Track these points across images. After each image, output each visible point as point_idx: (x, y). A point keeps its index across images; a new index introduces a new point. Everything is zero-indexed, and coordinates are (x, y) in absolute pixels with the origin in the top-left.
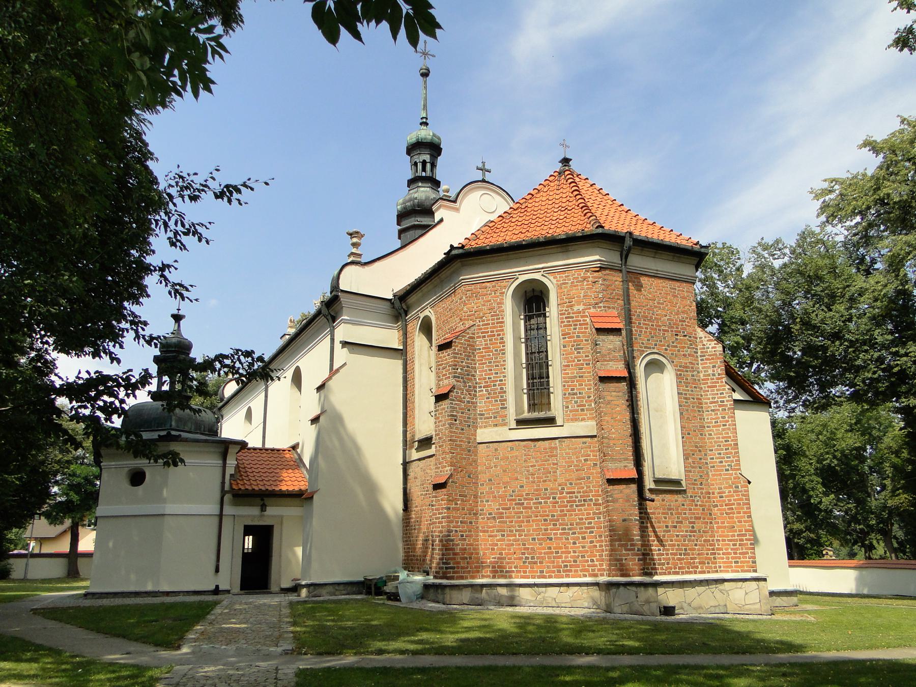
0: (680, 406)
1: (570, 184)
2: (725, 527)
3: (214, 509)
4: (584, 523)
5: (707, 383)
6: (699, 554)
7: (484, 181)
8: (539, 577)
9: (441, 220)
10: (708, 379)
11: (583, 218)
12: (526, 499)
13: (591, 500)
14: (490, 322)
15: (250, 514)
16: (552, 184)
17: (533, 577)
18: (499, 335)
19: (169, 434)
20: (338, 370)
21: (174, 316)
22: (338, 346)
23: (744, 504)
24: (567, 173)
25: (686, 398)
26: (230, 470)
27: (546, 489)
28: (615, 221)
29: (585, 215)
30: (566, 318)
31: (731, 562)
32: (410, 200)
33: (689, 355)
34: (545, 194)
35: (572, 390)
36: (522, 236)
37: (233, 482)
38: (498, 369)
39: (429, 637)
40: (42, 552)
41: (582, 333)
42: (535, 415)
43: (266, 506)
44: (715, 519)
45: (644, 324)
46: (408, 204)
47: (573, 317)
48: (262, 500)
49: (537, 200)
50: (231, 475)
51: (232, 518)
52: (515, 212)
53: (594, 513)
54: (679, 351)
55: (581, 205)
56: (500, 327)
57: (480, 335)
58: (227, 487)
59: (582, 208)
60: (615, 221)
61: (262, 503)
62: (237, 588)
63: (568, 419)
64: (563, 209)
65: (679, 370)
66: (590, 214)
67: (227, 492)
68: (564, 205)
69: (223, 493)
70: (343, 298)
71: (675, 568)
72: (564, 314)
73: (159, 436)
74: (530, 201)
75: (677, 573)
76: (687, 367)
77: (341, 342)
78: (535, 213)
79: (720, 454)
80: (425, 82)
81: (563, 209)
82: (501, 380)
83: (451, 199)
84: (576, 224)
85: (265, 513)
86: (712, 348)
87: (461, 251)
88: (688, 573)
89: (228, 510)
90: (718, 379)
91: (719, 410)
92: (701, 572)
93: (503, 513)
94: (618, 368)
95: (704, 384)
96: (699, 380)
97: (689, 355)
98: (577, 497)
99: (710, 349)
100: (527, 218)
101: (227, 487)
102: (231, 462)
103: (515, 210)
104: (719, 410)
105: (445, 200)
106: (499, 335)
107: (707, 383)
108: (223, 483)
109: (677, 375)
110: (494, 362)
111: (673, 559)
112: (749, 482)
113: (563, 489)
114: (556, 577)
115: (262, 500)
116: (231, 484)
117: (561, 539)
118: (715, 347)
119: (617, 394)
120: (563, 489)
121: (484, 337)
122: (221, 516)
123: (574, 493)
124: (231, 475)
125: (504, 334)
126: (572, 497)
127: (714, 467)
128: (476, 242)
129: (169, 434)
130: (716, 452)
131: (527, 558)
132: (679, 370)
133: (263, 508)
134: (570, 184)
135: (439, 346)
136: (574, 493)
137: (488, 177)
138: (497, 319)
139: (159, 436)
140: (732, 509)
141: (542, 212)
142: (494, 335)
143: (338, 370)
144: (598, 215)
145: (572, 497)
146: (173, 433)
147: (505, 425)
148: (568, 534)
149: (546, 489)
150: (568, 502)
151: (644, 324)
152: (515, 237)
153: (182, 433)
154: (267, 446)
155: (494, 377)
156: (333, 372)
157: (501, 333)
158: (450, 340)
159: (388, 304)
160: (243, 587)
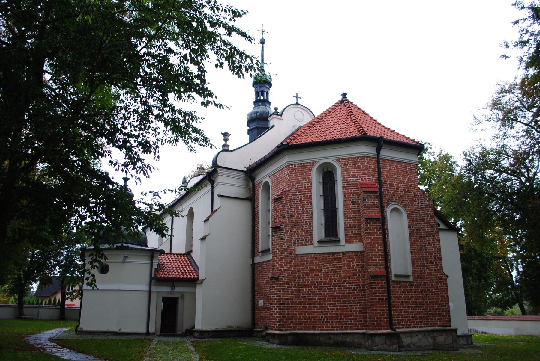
0: (410, 234)
1: (347, 108)
2: (434, 302)
3: (146, 287)
4: (357, 300)
5: (424, 221)
6: (420, 317)
7: (297, 104)
8: (331, 330)
9: (273, 126)
10: (425, 219)
11: (355, 128)
12: (323, 287)
13: (360, 287)
14: (304, 186)
15: (166, 290)
16: (337, 108)
17: (328, 330)
18: (309, 194)
19: (122, 245)
20: (216, 211)
21: (124, 179)
22: (216, 197)
23: (445, 289)
24: (345, 102)
25: (413, 230)
26: (155, 266)
27: (335, 281)
28: (373, 130)
29: (356, 126)
30: (346, 184)
31: (437, 321)
32: (254, 113)
33: (415, 205)
34: (333, 114)
35: (350, 225)
36: (321, 138)
37: (156, 273)
38: (308, 213)
39: (70, 357)
40: (38, 309)
41: (355, 193)
42: (329, 239)
43: (175, 286)
44: (429, 297)
45: (389, 188)
46: (254, 115)
47: (350, 184)
48: (173, 283)
49: (329, 117)
50: (155, 269)
51: (156, 292)
52: (317, 124)
53: (362, 295)
54: (409, 203)
55: (354, 121)
56: (309, 189)
57: (298, 193)
58: (153, 276)
59: (354, 122)
60: (373, 130)
61: (172, 284)
62: (159, 333)
63: (347, 241)
64: (344, 123)
65: (409, 214)
66: (360, 126)
67: (153, 278)
68: (344, 120)
69: (151, 279)
70: (219, 170)
71: (406, 325)
72: (345, 182)
73: (117, 246)
74: (325, 118)
75: (408, 328)
76: (414, 212)
77: (218, 195)
78: (328, 125)
79: (432, 261)
80: (263, 47)
81: (344, 123)
82: (310, 219)
83: (279, 114)
84: (352, 132)
85: (175, 291)
86: (427, 201)
87: (287, 146)
88: (413, 327)
89: (154, 288)
90: (430, 218)
91: (431, 236)
92: (420, 327)
93: (310, 294)
94: (375, 213)
95: (422, 221)
96: (420, 219)
97: (415, 205)
98: (352, 285)
99: (426, 202)
100: (324, 128)
101: (153, 276)
102: (156, 262)
103: (316, 122)
104: (431, 236)
105: (275, 114)
106: (309, 194)
107: (424, 221)
108: (151, 273)
109: (408, 216)
110: (306, 209)
111: (405, 320)
112: (448, 277)
113: (344, 281)
114: (340, 330)
115: (173, 283)
116: (155, 274)
117: (344, 309)
118: (429, 201)
119: (375, 228)
120: (345, 281)
121: (300, 194)
122: (150, 292)
123: (351, 283)
124: (155, 269)
125: (311, 193)
126: (350, 286)
127: (428, 268)
128: (296, 141)
129: (122, 245)
130: (435, 266)
131: (324, 319)
132: (409, 214)
133: (173, 287)
134: (347, 108)
135: (275, 199)
136: (351, 283)
137: (300, 101)
138: (307, 184)
139: (117, 246)
140: (438, 291)
141: (332, 124)
142: (306, 194)
143: (216, 211)
144: (363, 126)
145: (350, 286)
146: (124, 245)
147: (312, 244)
148: (347, 306)
149: (335, 281)
150: (347, 288)
151: (389, 188)
152: (317, 138)
153: (129, 245)
154: (173, 252)
155: (306, 217)
156: (213, 212)
157: (310, 192)
158: (281, 196)
159: (243, 173)
160: (162, 331)
